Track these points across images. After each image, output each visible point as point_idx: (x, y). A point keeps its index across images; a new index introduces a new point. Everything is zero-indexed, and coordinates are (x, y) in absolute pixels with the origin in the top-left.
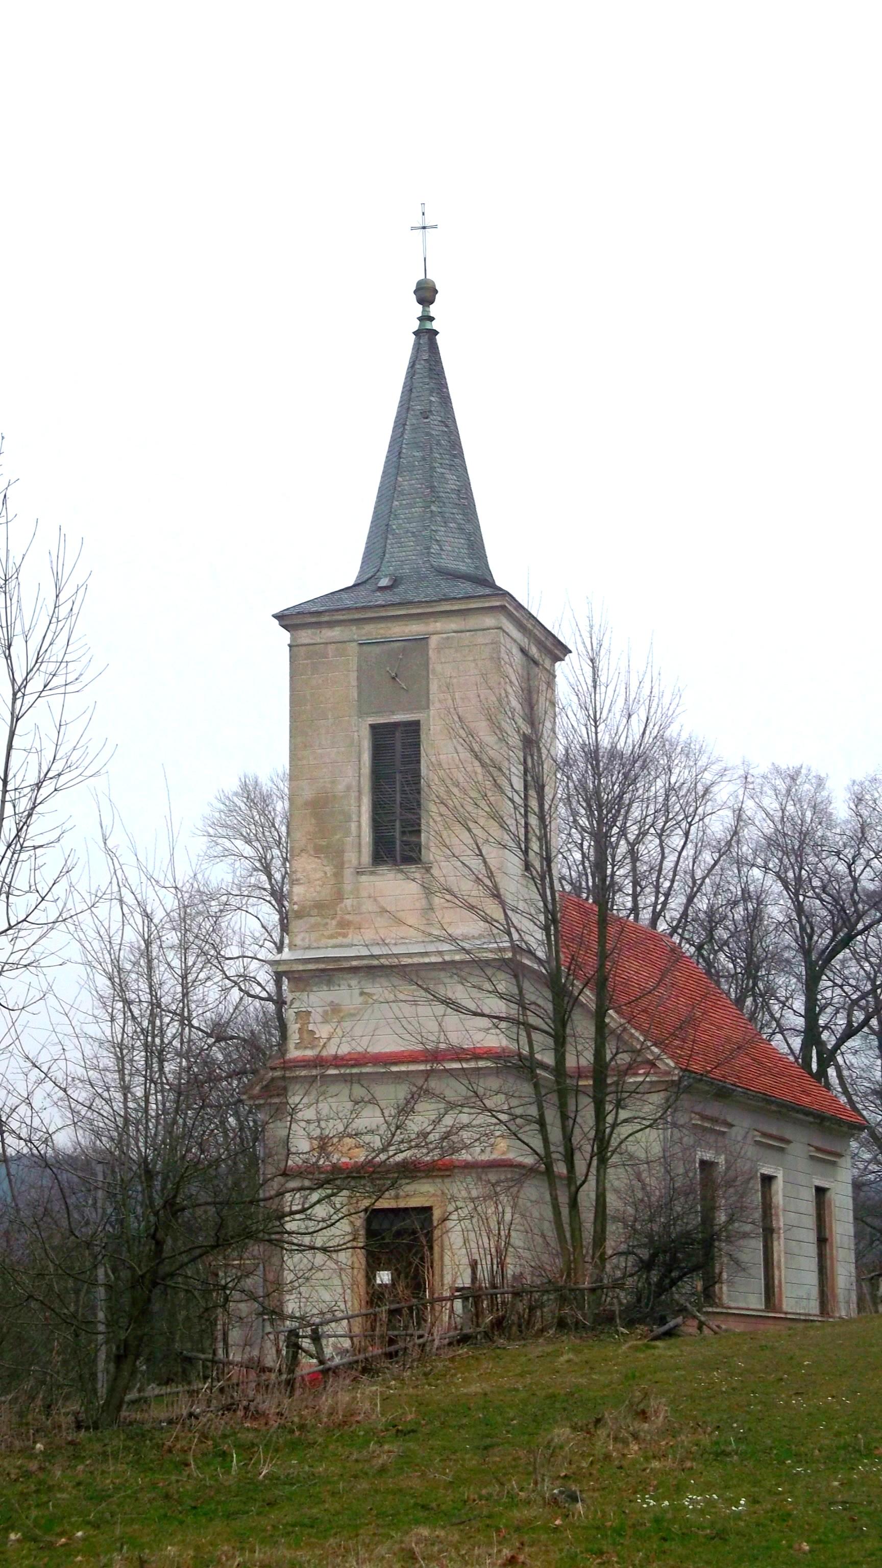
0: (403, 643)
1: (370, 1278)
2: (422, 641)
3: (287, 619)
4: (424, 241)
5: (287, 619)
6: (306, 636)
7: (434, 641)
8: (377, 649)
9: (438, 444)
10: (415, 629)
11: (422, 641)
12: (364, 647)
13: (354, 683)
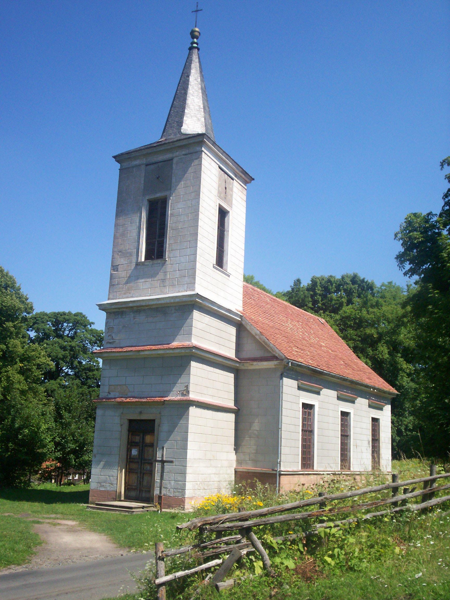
0: (163, 163)
1: (129, 451)
2: (172, 159)
3: (118, 158)
4: (197, 16)
5: (118, 158)
6: (125, 165)
7: (175, 161)
8: (152, 167)
9: (193, 88)
10: (168, 156)
11: (172, 159)
12: (148, 167)
13: (143, 182)
